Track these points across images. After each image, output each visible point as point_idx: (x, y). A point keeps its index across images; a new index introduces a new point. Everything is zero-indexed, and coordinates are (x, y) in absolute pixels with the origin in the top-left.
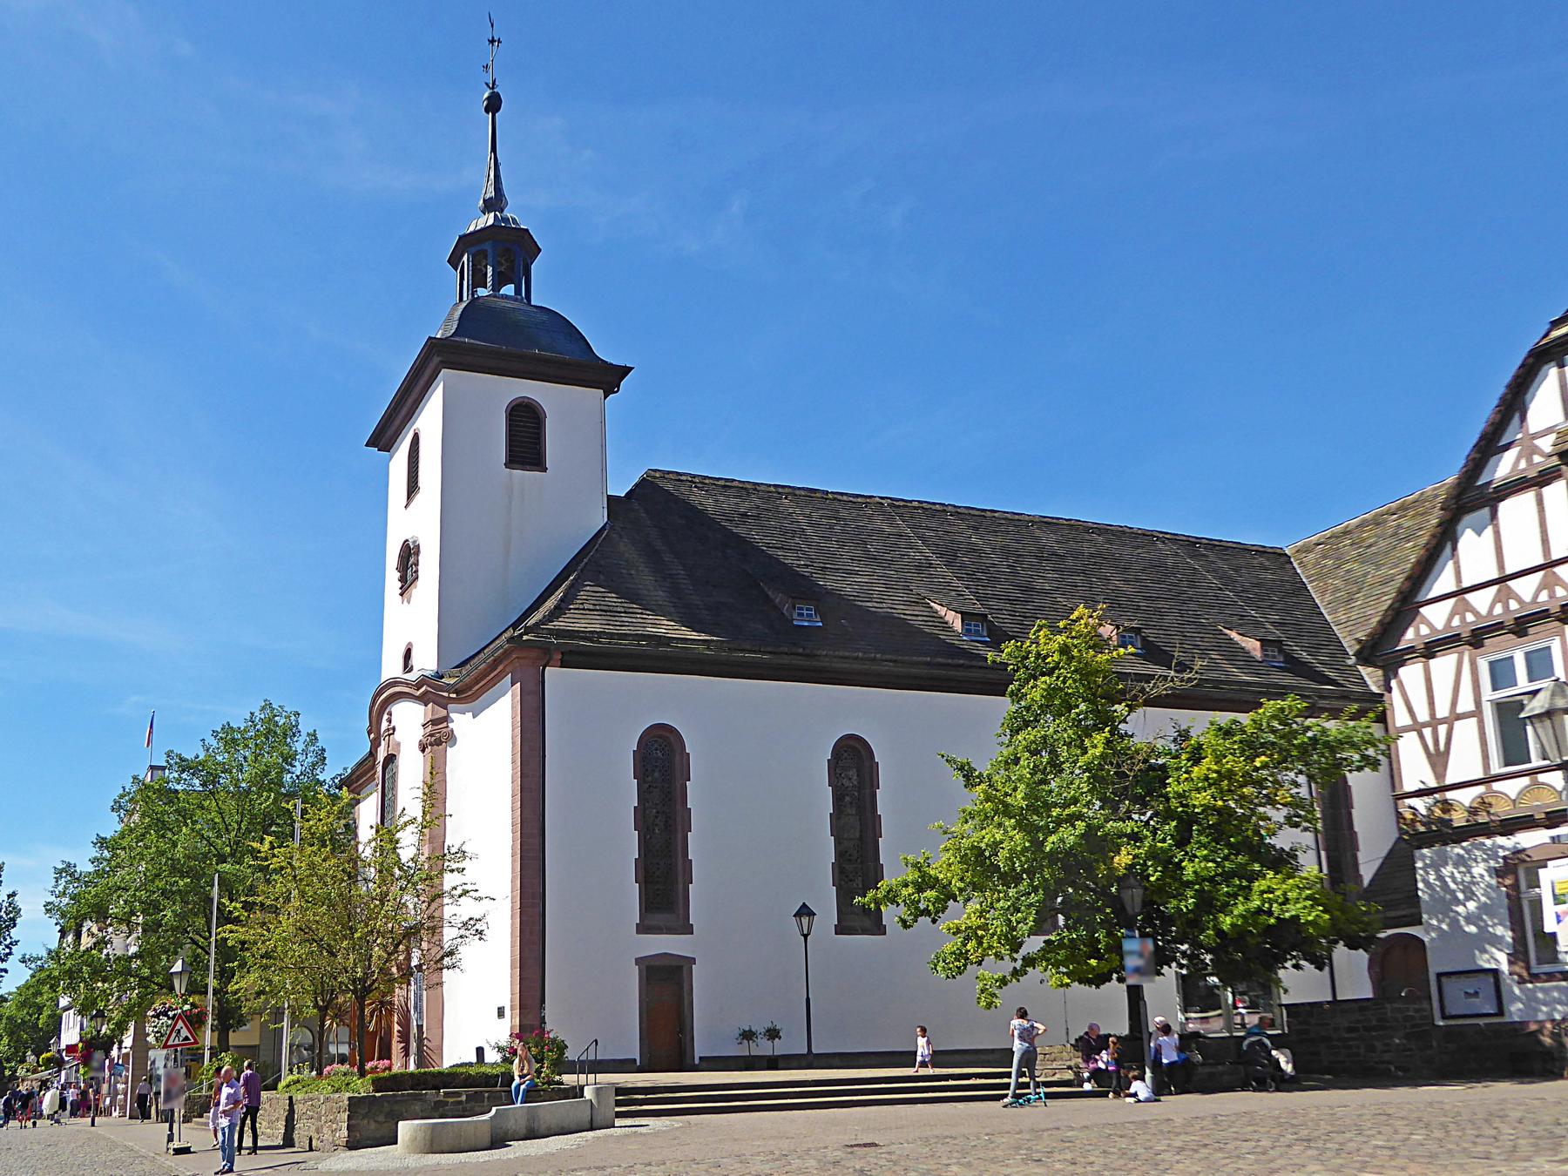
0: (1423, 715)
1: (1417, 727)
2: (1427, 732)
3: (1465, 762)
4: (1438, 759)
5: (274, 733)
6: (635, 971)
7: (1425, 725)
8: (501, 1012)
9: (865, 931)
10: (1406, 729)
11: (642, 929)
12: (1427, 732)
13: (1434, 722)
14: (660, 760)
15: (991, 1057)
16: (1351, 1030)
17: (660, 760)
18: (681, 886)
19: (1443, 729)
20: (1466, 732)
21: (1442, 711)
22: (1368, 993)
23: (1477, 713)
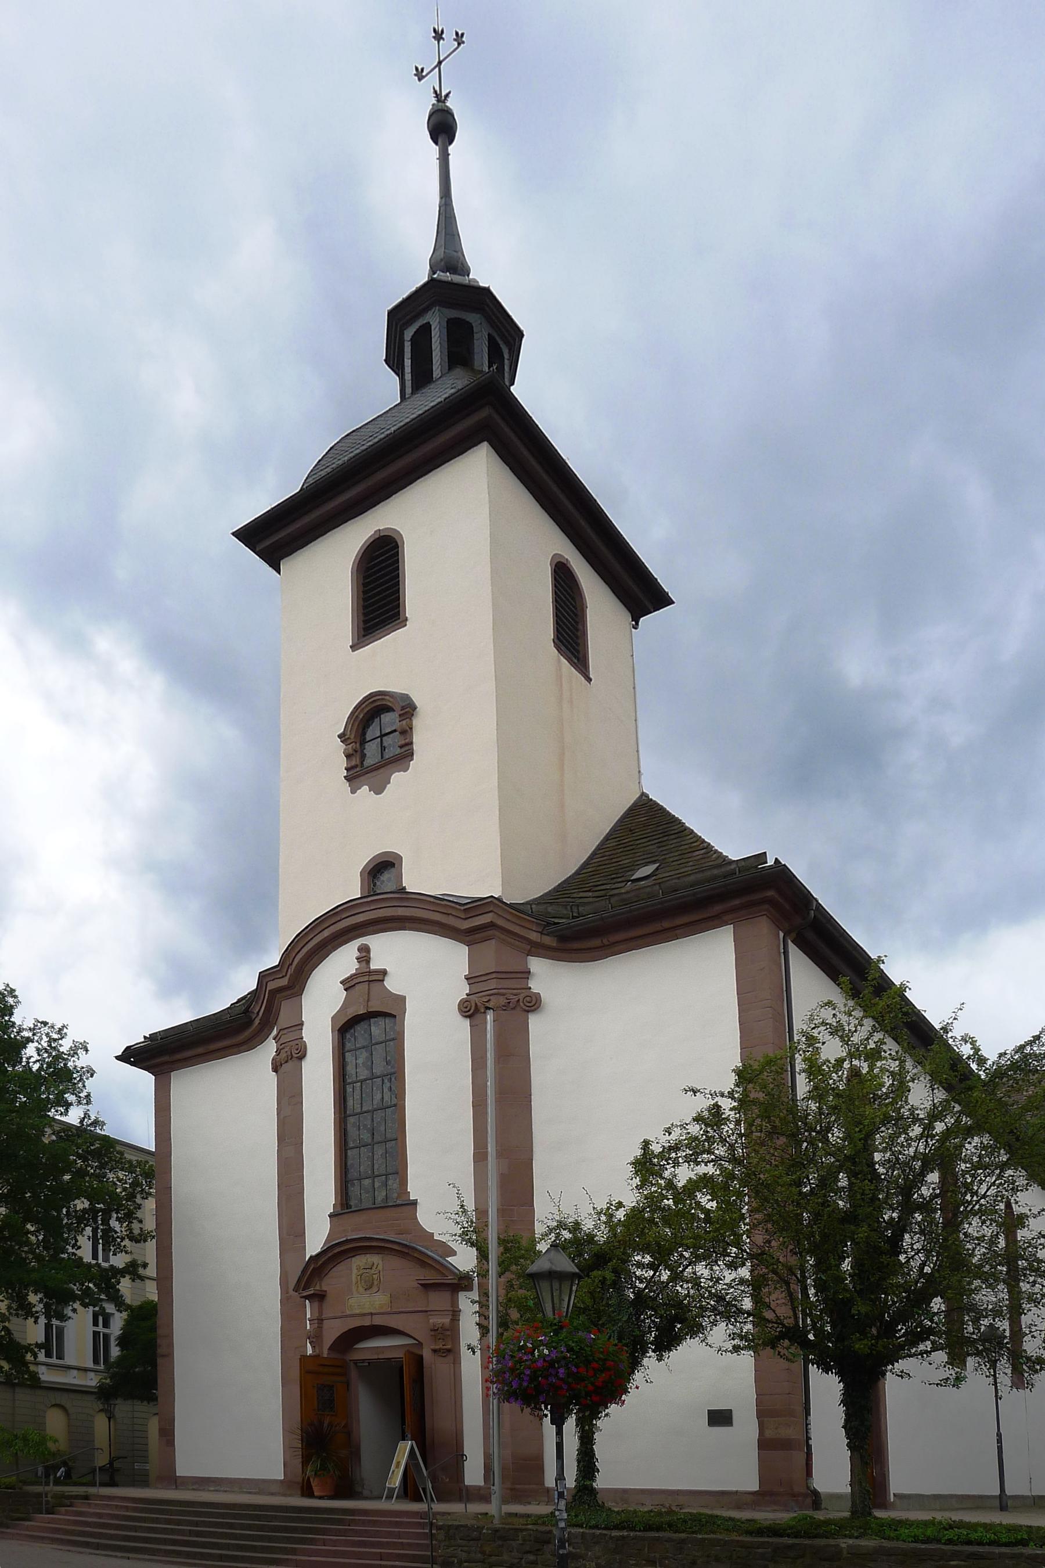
5: (378, 789)
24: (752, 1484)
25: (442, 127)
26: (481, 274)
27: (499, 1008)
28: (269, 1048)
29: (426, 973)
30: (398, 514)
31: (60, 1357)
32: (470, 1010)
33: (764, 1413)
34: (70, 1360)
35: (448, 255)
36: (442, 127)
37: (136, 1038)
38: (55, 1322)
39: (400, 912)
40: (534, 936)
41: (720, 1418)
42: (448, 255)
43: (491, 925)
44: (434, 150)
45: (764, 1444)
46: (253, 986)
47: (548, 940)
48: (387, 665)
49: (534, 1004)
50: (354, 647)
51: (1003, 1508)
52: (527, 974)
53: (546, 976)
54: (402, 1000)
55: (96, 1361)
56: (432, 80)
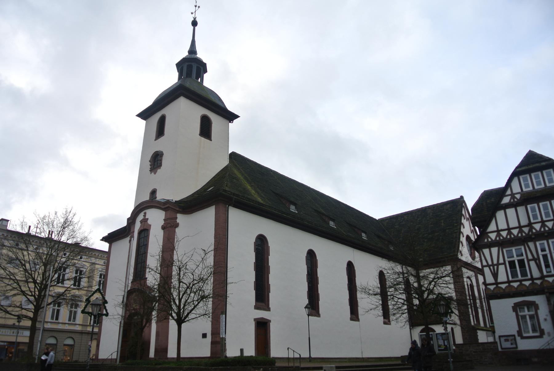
0: (490, 263)
1: (488, 266)
2: (491, 267)
3: (502, 277)
4: (495, 275)
5: (155, 173)
6: (254, 323)
7: (491, 265)
8: (204, 336)
9: (315, 316)
10: (93, 329)
11: (256, 308)
12: (491, 267)
13: (493, 265)
14: (261, 246)
15: (346, 360)
16: (474, 352)
17: (261, 246)
18: (266, 293)
19: (496, 267)
20: (502, 268)
21: (495, 262)
22: (480, 341)
23: (504, 263)
24: (209, 355)
25: (194, 23)
26: (199, 55)
27: (170, 227)
28: (128, 238)
29: (156, 218)
30: (166, 111)
31: (57, 319)
32: (163, 228)
33: (213, 334)
34: (60, 320)
35: (192, 50)
36: (194, 23)
37: (106, 234)
38: (73, 309)
39: (152, 204)
40: (177, 209)
41: (204, 336)
42: (192, 50)
43: (169, 207)
44: (192, 27)
45: (213, 343)
46: (504, 186)
47: (180, 210)
48: (160, 145)
49: (177, 225)
50: (155, 140)
51: (310, 361)
52: (177, 218)
53: (181, 218)
54: (150, 226)
55: (70, 320)
56: (194, 14)
